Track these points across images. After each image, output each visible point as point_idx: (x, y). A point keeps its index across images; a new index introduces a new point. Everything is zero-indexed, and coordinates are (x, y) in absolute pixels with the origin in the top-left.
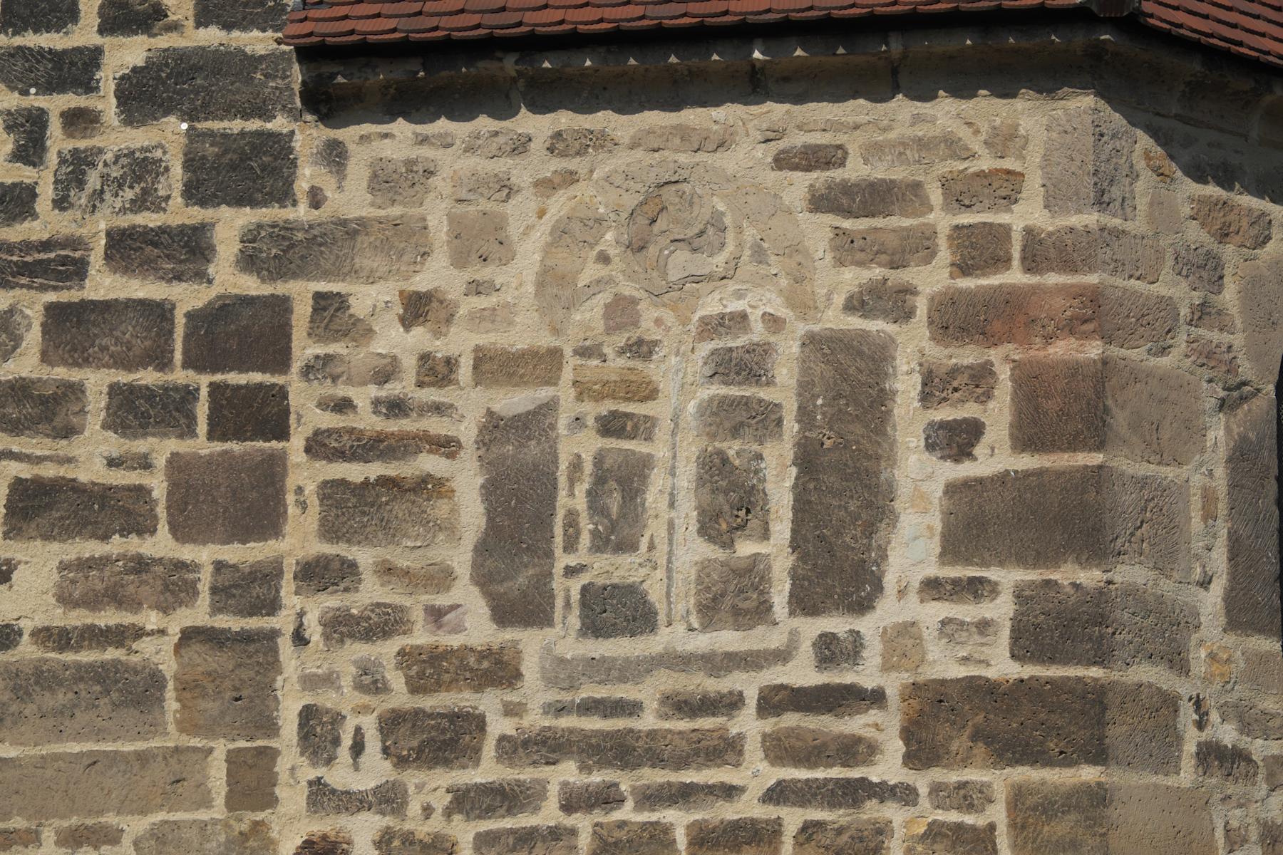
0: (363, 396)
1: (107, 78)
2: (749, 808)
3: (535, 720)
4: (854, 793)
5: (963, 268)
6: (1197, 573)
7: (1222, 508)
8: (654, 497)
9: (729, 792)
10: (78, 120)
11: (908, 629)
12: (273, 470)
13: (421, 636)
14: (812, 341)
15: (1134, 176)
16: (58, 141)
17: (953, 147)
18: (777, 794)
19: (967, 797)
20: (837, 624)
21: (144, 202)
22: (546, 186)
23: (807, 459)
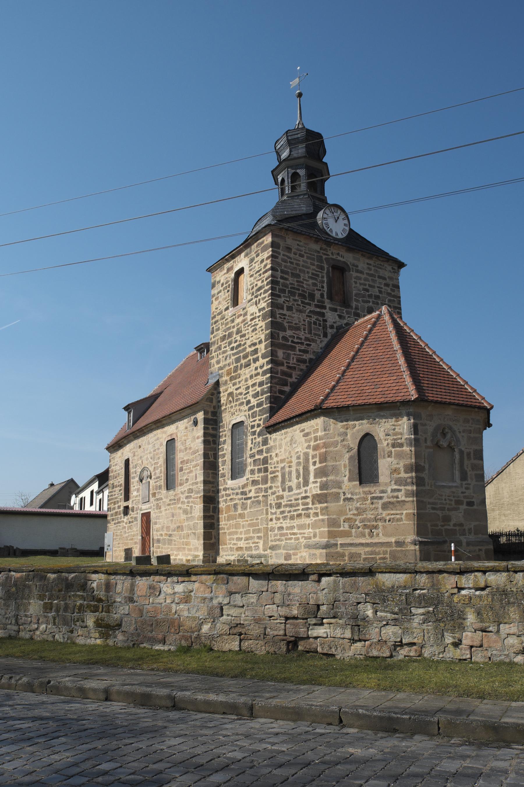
1: (257, 433)
2: (300, 512)
5: (315, 442)
6: (343, 475)
7: (348, 466)
8: (292, 475)
9: (299, 510)
12: (267, 476)
13: (277, 494)
14: (304, 453)
15: (330, 425)
16: (254, 441)
17: (313, 426)
18: (303, 510)
19: (316, 508)
20: (306, 488)
21: (259, 447)
22: (284, 438)
23: (303, 469)
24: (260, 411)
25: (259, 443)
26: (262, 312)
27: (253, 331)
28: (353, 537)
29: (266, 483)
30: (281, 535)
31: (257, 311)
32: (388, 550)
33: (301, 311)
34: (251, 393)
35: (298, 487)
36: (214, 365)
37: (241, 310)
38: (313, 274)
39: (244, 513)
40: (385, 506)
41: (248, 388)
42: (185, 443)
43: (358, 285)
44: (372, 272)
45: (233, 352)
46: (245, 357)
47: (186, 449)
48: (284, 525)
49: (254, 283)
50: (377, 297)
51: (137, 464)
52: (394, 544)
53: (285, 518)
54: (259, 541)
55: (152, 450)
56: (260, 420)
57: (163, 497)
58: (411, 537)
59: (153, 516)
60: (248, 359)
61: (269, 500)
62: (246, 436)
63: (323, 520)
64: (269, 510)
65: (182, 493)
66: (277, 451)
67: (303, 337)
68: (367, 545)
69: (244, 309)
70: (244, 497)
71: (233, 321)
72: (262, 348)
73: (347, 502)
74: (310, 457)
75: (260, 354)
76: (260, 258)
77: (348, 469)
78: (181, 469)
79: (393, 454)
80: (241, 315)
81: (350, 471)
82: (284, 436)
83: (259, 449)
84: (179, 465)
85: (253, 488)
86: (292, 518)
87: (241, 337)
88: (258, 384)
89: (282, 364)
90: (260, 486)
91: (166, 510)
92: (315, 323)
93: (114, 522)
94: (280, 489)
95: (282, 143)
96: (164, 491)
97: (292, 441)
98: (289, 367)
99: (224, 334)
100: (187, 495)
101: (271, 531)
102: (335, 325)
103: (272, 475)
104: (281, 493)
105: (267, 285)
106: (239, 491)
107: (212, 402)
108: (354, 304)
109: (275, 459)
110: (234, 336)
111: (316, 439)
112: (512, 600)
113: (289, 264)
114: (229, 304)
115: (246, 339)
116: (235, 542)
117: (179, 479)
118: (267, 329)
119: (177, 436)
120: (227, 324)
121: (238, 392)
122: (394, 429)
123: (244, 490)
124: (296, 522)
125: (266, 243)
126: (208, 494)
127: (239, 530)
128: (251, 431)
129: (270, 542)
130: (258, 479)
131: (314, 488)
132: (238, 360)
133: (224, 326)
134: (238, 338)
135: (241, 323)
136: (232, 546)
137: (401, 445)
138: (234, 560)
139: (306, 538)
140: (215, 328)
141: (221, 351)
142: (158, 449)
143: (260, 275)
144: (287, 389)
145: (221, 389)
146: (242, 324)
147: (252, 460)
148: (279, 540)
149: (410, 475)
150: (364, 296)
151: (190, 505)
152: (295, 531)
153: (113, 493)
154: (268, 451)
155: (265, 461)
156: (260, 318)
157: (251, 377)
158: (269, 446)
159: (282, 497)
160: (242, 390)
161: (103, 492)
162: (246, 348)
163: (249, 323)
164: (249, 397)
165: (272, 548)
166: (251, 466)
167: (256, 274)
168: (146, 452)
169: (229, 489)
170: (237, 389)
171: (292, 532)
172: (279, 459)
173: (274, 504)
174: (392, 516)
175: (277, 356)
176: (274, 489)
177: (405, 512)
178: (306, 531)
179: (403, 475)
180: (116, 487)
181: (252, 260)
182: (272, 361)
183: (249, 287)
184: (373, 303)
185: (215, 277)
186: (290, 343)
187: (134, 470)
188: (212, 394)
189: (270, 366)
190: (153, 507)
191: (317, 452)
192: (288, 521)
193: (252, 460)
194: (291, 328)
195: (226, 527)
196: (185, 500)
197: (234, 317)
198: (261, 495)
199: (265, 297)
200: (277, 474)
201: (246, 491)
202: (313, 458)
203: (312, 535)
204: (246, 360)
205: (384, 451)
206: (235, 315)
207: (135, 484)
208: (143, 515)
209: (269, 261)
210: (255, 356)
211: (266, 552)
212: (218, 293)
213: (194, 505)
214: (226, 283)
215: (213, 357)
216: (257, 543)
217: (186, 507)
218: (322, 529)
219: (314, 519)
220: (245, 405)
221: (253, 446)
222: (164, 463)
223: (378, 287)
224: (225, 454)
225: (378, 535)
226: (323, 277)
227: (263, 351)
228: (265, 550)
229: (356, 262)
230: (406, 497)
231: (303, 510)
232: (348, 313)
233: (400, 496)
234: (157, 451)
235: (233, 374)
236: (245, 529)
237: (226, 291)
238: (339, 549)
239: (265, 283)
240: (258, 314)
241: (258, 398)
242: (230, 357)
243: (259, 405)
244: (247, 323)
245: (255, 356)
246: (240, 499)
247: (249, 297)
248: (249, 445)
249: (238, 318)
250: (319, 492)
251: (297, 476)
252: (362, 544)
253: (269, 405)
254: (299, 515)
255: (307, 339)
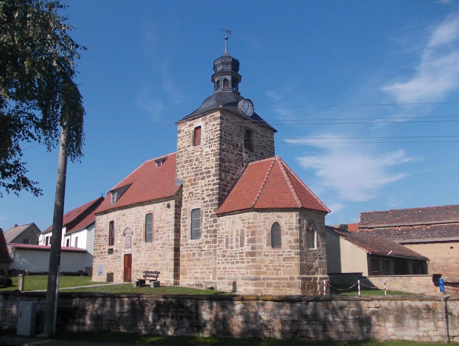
0: (220, 235)
1: (209, 216)
2: (238, 260)
3: (228, 255)
4: (243, 259)
5: (248, 224)
8: (233, 240)
10: (208, 219)
11: (245, 248)
12: (216, 240)
13: (223, 250)
16: (207, 220)
18: (240, 259)
19: (248, 259)
20: (242, 248)
21: (211, 223)
22: (228, 221)
23: (241, 237)
24: (211, 204)
25: (211, 221)
26: (213, 152)
27: (207, 161)
28: (268, 275)
29: (216, 243)
30: (225, 272)
31: (210, 151)
32: (286, 282)
33: (232, 153)
34: (205, 194)
35: (237, 247)
36: (179, 175)
37: (199, 149)
38: (238, 134)
39: (200, 259)
40: (284, 259)
41: (203, 191)
42: (161, 217)
43: (257, 140)
44: (263, 134)
45: (193, 170)
46: (201, 174)
47: (161, 220)
48: (227, 267)
49: (208, 136)
50: (265, 147)
51: (121, 225)
52: (289, 279)
53: (227, 263)
54: (210, 274)
55: (134, 218)
56: (212, 209)
57: (142, 246)
58: (297, 275)
59: (133, 257)
60: (203, 175)
61: (217, 252)
62: (202, 216)
63: (253, 266)
64: (217, 258)
65: (157, 244)
66: (223, 227)
67: (233, 167)
68: (276, 279)
69: (201, 148)
70: (200, 249)
71: (193, 153)
72: (213, 171)
73: (265, 257)
74: (245, 232)
75: (211, 174)
76: (212, 123)
77: (266, 239)
78: (157, 231)
79: (289, 233)
80: (199, 151)
81: (267, 240)
82: (228, 219)
83: (211, 224)
84: (155, 228)
85: (207, 245)
86: (233, 263)
87: (199, 163)
88: (210, 190)
89: (224, 181)
90: (211, 244)
91: (144, 253)
92: (238, 160)
93: (99, 257)
94: (225, 247)
95: (218, 62)
96: (143, 243)
97: (233, 222)
98: (227, 182)
99: (187, 159)
100: (161, 246)
101: (218, 269)
102: (247, 161)
103: (220, 239)
104: (225, 249)
105: (217, 138)
106: (197, 246)
107: (179, 196)
108: (255, 150)
109: (222, 231)
110: (194, 161)
111: (249, 223)
112: (390, 312)
113: (227, 128)
114: (191, 144)
115: (202, 165)
116: (193, 274)
117: (156, 236)
118: (216, 161)
119: (154, 212)
120: (189, 154)
121: (196, 192)
122: (289, 221)
123: (200, 246)
124: (235, 265)
125: (216, 116)
126: (176, 247)
127: (196, 268)
128: (205, 214)
129: (217, 275)
130: (210, 240)
131: (247, 248)
132: (196, 175)
133: (186, 155)
134: (197, 163)
135: (199, 155)
136: (191, 276)
137: (292, 229)
138: (193, 285)
139: (241, 274)
140: (180, 155)
141: (184, 169)
142: (139, 218)
143: (212, 132)
144: (226, 193)
145: (183, 189)
146: (200, 156)
147: (206, 230)
148: (224, 274)
149: (296, 244)
150: (259, 146)
151: (164, 252)
152: (235, 270)
153: (99, 240)
154: (217, 226)
155: (215, 231)
156: (212, 155)
157: (205, 185)
158: (217, 223)
159: (226, 252)
160: (199, 191)
161: (71, 235)
162: (202, 169)
163: (205, 156)
164: (204, 196)
165: (219, 279)
166: (205, 233)
167: (209, 131)
168: (129, 219)
169: (189, 244)
170: (195, 191)
171: (232, 270)
172: (224, 231)
173: (220, 255)
174: (288, 265)
175: (222, 177)
176: (221, 247)
177: (294, 263)
178: (242, 270)
179: (293, 244)
180: (101, 236)
181: (206, 124)
182: (220, 179)
183: (205, 137)
184: (263, 150)
185: (181, 128)
186: (227, 170)
187: (118, 228)
188: (179, 192)
189: (218, 181)
190: (134, 251)
191: (250, 230)
192: (230, 264)
193: (206, 230)
194: (228, 162)
195: (187, 265)
196: (159, 249)
197: (194, 151)
198: (212, 249)
199: (216, 145)
200: (223, 239)
201: (201, 247)
202: (247, 233)
203: (245, 273)
204: (202, 176)
205: (284, 232)
206: (195, 150)
207: (119, 236)
208: (125, 255)
209: (218, 126)
210: (208, 175)
211: (215, 281)
212: (183, 137)
213: (166, 252)
214: (188, 132)
215: (179, 171)
216: (209, 275)
217: (160, 253)
218: (252, 270)
219: (247, 264)
220: (201, 200)
221: (206, 222)
222: (144, 226)
223: (265, 142)
224: (187, 225)
225: (280, 274)
226: (242, 136)
227: (214, 173)
228: (214, 279)
229: (256, 129)
230: (295, 255)
231: (240, 259)
232: (253, 155)
233: (292, 255)
234: (138, 219)
235: (192, 182)
236: (201, 267)
237: (188, 136)
238: (262, 281)
239: (216, 137)
240: (210, 153)
241: (210, 197)
242: (191, 173)
243: (211, 201)
244: (203, 156)
245: (208, 175)
246: (197, 251)
247: (205, 143)
248: (204, 221)
249: (197, 152)
250: (250, 251)
251: (236, 241)
252: (273, 279)
253: (218, 202)
254: (237, 262)
255: (235, 168)
